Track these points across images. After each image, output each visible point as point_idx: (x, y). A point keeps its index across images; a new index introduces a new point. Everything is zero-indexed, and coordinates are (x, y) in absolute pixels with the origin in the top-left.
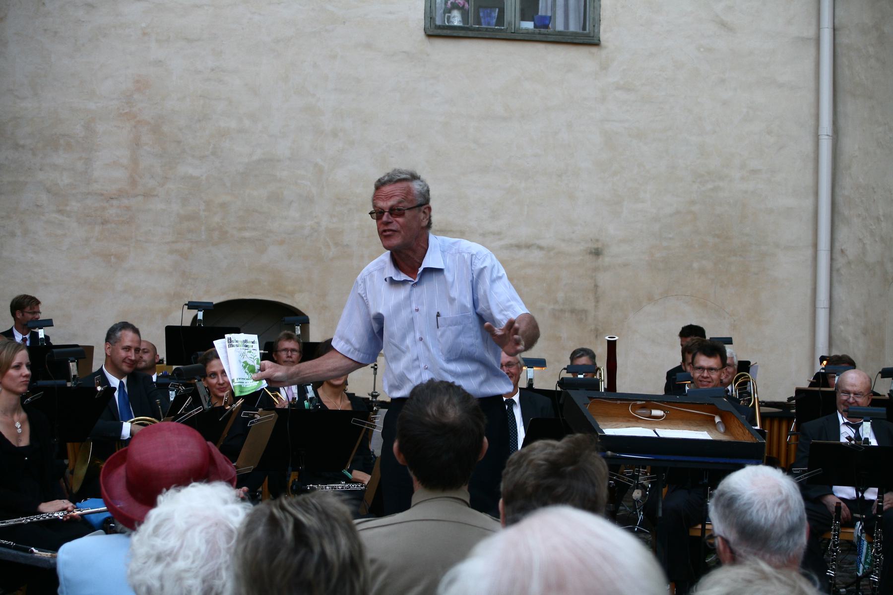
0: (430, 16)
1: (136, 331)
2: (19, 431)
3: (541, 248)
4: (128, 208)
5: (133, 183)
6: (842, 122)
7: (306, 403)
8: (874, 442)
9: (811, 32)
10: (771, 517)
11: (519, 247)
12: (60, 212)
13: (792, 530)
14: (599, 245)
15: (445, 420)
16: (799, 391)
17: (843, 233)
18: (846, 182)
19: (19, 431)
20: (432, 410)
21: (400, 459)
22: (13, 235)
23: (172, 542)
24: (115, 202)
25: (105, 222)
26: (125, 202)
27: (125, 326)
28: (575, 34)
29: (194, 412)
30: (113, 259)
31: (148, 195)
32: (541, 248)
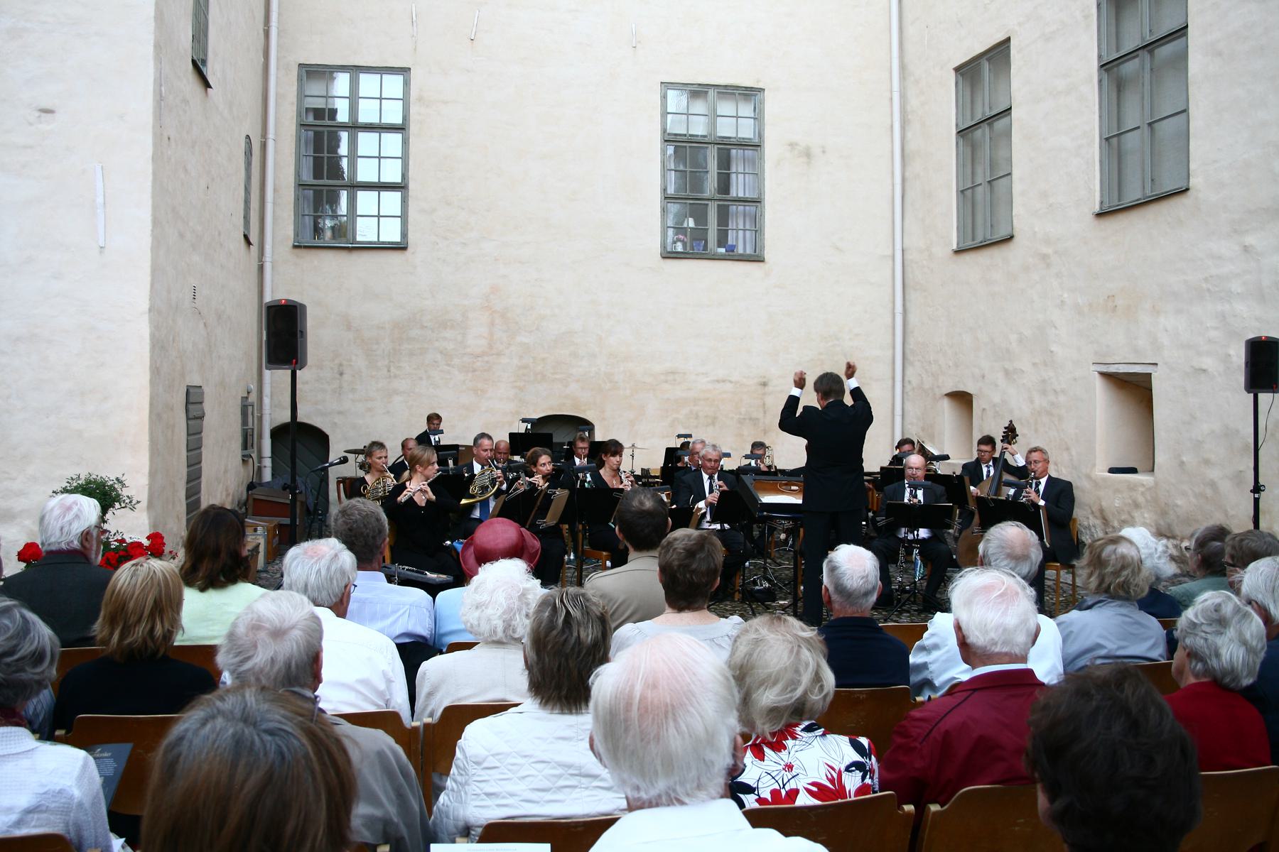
0: (664, 246)
1: (490, 438)
5: (491, 347)
6: (908, 304)
9: (889, 252)
10: (855, 585)
13: (867, 594)
16: (882, 468)
17: (909, 371)
20: (635, 503)
22: (421, 379)
23: (485, 598)
26: (486, 358)
27: (483, 435)
31: (499, 354)
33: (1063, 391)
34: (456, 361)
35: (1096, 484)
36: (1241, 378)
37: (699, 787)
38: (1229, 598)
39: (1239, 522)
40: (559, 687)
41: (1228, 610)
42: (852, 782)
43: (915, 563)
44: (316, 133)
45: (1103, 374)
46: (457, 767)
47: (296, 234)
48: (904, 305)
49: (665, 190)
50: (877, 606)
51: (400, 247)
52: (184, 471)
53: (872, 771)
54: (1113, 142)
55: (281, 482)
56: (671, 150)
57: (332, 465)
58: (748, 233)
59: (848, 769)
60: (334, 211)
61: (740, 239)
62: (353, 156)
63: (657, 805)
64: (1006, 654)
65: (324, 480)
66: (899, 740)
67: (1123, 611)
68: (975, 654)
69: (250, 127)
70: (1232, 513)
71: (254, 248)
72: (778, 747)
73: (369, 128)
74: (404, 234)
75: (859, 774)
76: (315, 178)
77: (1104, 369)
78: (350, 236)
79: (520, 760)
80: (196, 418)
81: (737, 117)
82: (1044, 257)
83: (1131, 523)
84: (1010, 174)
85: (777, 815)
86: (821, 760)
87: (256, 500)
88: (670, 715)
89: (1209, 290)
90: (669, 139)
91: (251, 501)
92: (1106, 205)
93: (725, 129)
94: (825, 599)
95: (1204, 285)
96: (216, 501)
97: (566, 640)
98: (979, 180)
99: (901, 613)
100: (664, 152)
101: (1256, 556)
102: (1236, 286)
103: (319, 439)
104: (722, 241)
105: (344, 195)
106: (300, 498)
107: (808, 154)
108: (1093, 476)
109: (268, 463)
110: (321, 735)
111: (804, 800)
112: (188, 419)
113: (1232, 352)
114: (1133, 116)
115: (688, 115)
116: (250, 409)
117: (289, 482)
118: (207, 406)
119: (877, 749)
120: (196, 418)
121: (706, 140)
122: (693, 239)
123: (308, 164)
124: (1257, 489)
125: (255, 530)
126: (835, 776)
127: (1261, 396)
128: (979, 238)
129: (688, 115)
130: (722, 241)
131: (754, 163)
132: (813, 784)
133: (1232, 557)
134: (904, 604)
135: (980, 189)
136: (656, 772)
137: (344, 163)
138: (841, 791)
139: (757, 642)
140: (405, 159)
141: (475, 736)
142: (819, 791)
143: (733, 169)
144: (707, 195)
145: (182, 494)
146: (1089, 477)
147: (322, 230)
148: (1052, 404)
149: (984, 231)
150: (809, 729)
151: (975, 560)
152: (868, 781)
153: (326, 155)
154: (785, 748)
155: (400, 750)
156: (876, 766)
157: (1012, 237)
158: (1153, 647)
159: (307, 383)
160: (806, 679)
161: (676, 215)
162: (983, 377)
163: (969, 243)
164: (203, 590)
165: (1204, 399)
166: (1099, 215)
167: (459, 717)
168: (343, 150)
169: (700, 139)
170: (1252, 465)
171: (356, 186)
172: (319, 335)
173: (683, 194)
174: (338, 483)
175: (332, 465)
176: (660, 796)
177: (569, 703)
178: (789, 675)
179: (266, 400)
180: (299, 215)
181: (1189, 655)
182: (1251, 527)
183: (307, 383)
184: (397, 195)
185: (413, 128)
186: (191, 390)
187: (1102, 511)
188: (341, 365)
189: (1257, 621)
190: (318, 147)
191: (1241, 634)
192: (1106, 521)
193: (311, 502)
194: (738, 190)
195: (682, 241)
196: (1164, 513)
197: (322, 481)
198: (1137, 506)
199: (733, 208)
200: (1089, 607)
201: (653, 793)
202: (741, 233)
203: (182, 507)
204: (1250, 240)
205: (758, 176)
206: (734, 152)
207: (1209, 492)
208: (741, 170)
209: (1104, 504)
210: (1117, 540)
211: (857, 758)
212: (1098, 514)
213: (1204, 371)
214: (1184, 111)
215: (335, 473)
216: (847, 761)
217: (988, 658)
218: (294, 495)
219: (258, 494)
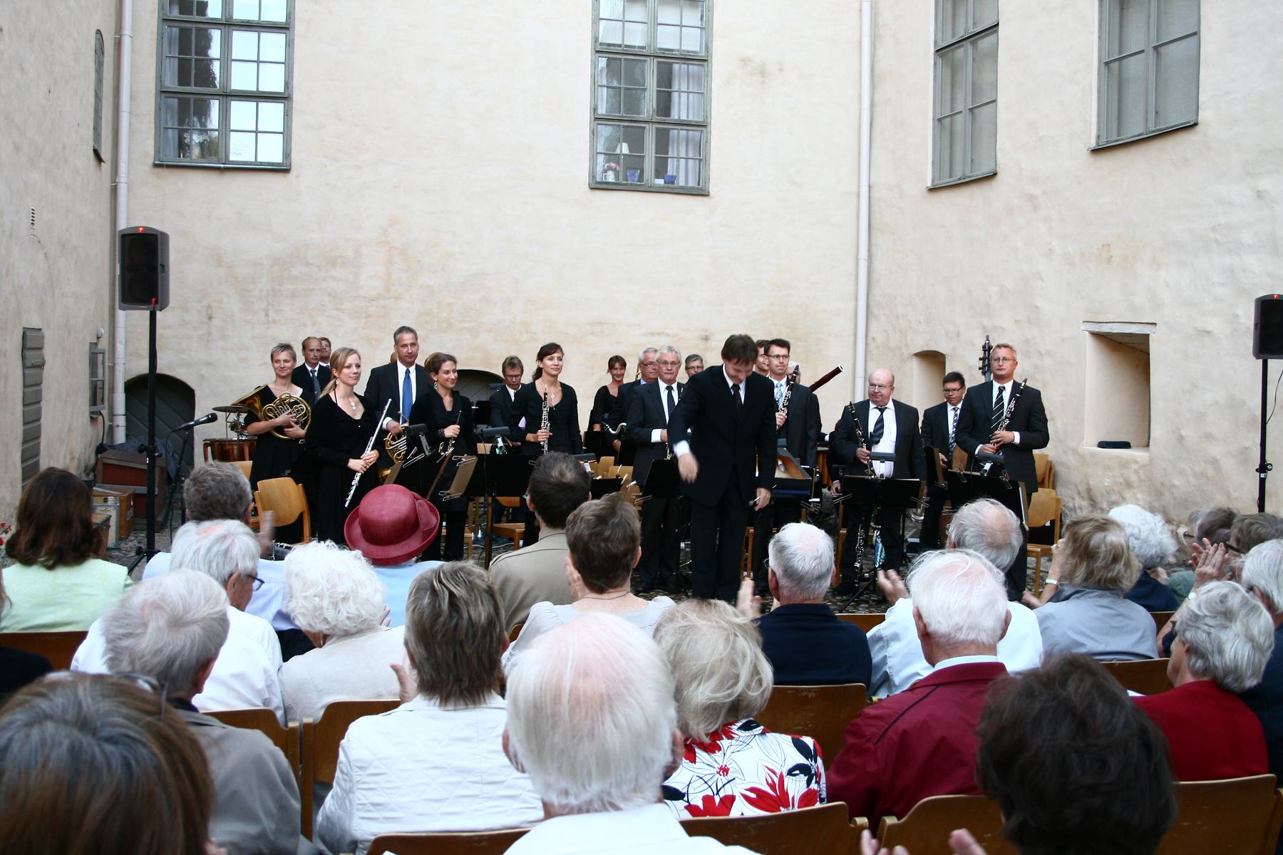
0: (592, 175)
4: (384, 307)
6: (874, 250)
8: (875, 699)
9: (854, 189)
10: (807, 567)
12: (338, 309)
13: (820, 577)
17: (874, 326)
18: (877, 291)
20: (555, 473)
21: (531, 508)
22: (305, 325)
25: (368, 316)
26: (382, 302)
28: (693, 188)
31: (397, 298)
33: (1049, 353)
34: (347, 305)
35: (1082, 458)
36: (1249, 342)
37: (637, 789)
38: (1237, 590)
39: (1245, 504)
40: (458, 680)
41: (1235, 601)
42: (796, 787)
43: (874, 547)
44: (182, 31)
45: (1094, 334)
46: (342, 772)
47: (157, 151)
48: (869, 251)
49: (595, 109)
50: (836, 590)
51: (282, 169)
52: (19, 429)
53: (818, 775)
54: (1113, 66)
55: (136, 443)
56: (603, 62)
57: (198, 423)
58: (690, 162)
59: (790, 773)
60: (203, 124)
61: (680, 169)
62: (226, 58)
63: (588, 811)
64: (973, 642)
65: (189, 441)
66: (851, 740)
67: (1105, 601)
68: (938, 644)
69: (101, 19)
70: (1235, 495)
71: (106, 167)
72: (712, 748)
73: (247, 26)
74: (287, 154)
75: (803, 778)
76: (180, 84)
77: (1097, 328)
78: (222, 155)
79: (415, 765)
80: (34, 367)
81: (681, 26)
82: (1032, 198)
83: (1122, 500)
84: (994, 101)
85: (709, 821)
86: (762, 762)
87: (107, 465)
88: (606, 706)
89: (1216, 241)
90: (601, 50)
91: (100, 467)
92: (1103, 140)
93: (667, 40)
94: (771, 585)
95: (1212, 235)
96: (59, 465)
97: (456, 625)
98: (959, 107)
99: (858, 603)
100: (594, 65)
101: (1261, 540)
102: (1247, 237)
103: (182, 394)
104: (661, 170)
105: (215, 105)
106: (160, 462)
107: (762, 72)
108: (1080, 450)
109: (121, 421)
110: (170, 732)
111: (741, 810)
112: (25, 367)
113: (1240, 312)
114: (1137, 38)
115: (624, 21)
116: (100, 357)
117: (146, 444)
118: (48, 352)
119: (825, 750)
120: (34, 367)
121: (645, 52)
122: (627, 168)
123: (172, 67)
124: (1263, 467)
125: (106, 500)
126: (776, 780)
127: (1271, 362)
128: (958, 174)
129: (624, 21)
130: (661, 170)
131: (699, 80)
132: (752, 790)
133: (1238, 541)
134: (862, 594)
135: (959, 118)
136: (589, 773)
137: (216, 67)
138: (783, 799)
139: (685, 631)
140: (288, 63)
141: (360, 737)
142: (759, 798)
143: (675, 87)
144: (644, 116)
145: (17, 457)
146: (1075, 452)
147: (189, 146)
148: (1036, 367)
149: (963, 168)
150: (746, 727)
151: (934, 538)
152: (814, 786)
153: (194, 57)
154: (719, 749)
155: (280, 753)
156: (822, 770)
157: (995, 174)
158: (1140, 641)
159: (169, 327)
160: (745, 672)
161: (608, 139)
162: (958, 335)
163: (946, 180)
164: (50, 568)
165: (1206, 365)
166: (1095, 151)
167: (342, 715)
168: (215, 51)
169: (637, 51)
170: (1258, 441)
171: (230, 96)
172: (183, 271)
173: (616, 115)
174: (206, 446)
175: (198, 423)
176: (590, 802)
177: (471, 695)
178: (723, 669)
179: (120, 347)
180: (160, 128)
181: (1188, 651)
182: (1255, 510)
183: (169, 327)
184: (278, 108)
185: (299, 28)
186: (28, 333)
187: (1089, 490)
188: (209, 307)
189: (1266, 616)
190: (184, 47)
191: (1247, 628)
192: (1093, 503)
193: (172, 467)
194: (680, 110)
195: (615, 170)
196: (1159, 494)
197: (185, 442)
198: (1129, 485)
199: (673, 133)
200: (1067, 598)
201: (584, 797)
202: (682, 162)
203: (17, 472)
204: (1265, 184)
205: (704, 96)
206: (676, 67)
207: (1210, 471)
208: (684, 88)
209: (1092, 482)
210: (1105, 525)
211: (801, 760)
212: (1085, 494)
213: (1209, 332)
214: (1195, 34)
215: (202, 433)
216: (790, 765)
217: (953, 647)
218: (153, 459)
219: (110, 458)
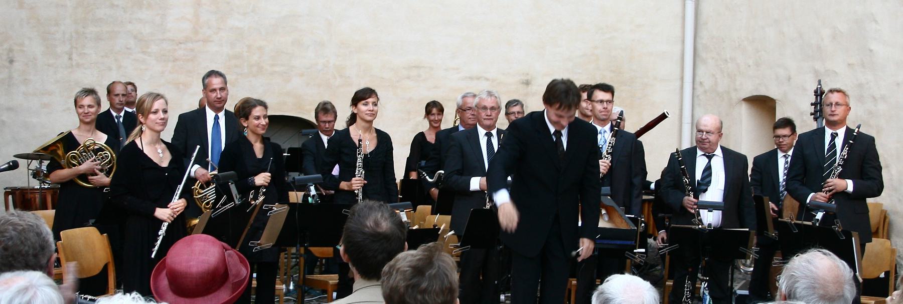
2: (161, 155)
3: (487, 79)
4: (192, 50)
7: (310, 199)
11: (471, 78)
12: (144, 52)
14: (529, 78)
15: (380, 230)
19: (161, 155)
20: (370, 223)
21: (345, 258)
22: (110, 69)
24: (183, 46)
25: (175, 60)
26: (190, 45)
29: (228, 206)
30: (181, 87)
31: (206, 41)
32: (487, 79)
34: (154, 48)
